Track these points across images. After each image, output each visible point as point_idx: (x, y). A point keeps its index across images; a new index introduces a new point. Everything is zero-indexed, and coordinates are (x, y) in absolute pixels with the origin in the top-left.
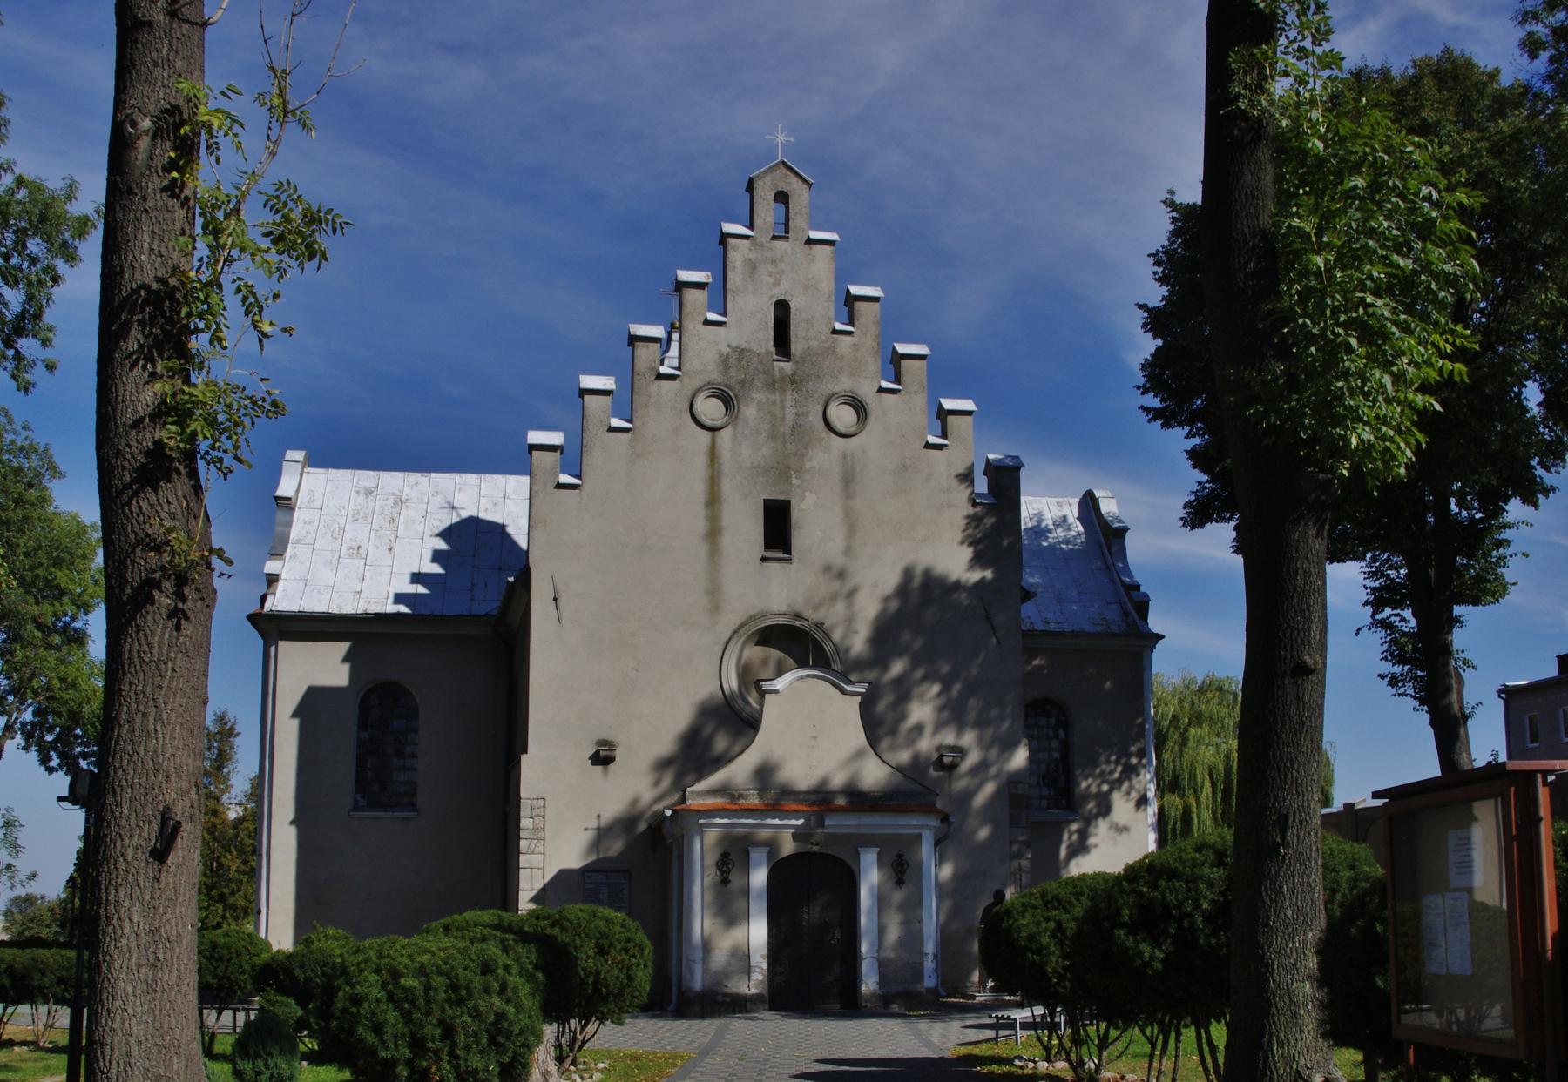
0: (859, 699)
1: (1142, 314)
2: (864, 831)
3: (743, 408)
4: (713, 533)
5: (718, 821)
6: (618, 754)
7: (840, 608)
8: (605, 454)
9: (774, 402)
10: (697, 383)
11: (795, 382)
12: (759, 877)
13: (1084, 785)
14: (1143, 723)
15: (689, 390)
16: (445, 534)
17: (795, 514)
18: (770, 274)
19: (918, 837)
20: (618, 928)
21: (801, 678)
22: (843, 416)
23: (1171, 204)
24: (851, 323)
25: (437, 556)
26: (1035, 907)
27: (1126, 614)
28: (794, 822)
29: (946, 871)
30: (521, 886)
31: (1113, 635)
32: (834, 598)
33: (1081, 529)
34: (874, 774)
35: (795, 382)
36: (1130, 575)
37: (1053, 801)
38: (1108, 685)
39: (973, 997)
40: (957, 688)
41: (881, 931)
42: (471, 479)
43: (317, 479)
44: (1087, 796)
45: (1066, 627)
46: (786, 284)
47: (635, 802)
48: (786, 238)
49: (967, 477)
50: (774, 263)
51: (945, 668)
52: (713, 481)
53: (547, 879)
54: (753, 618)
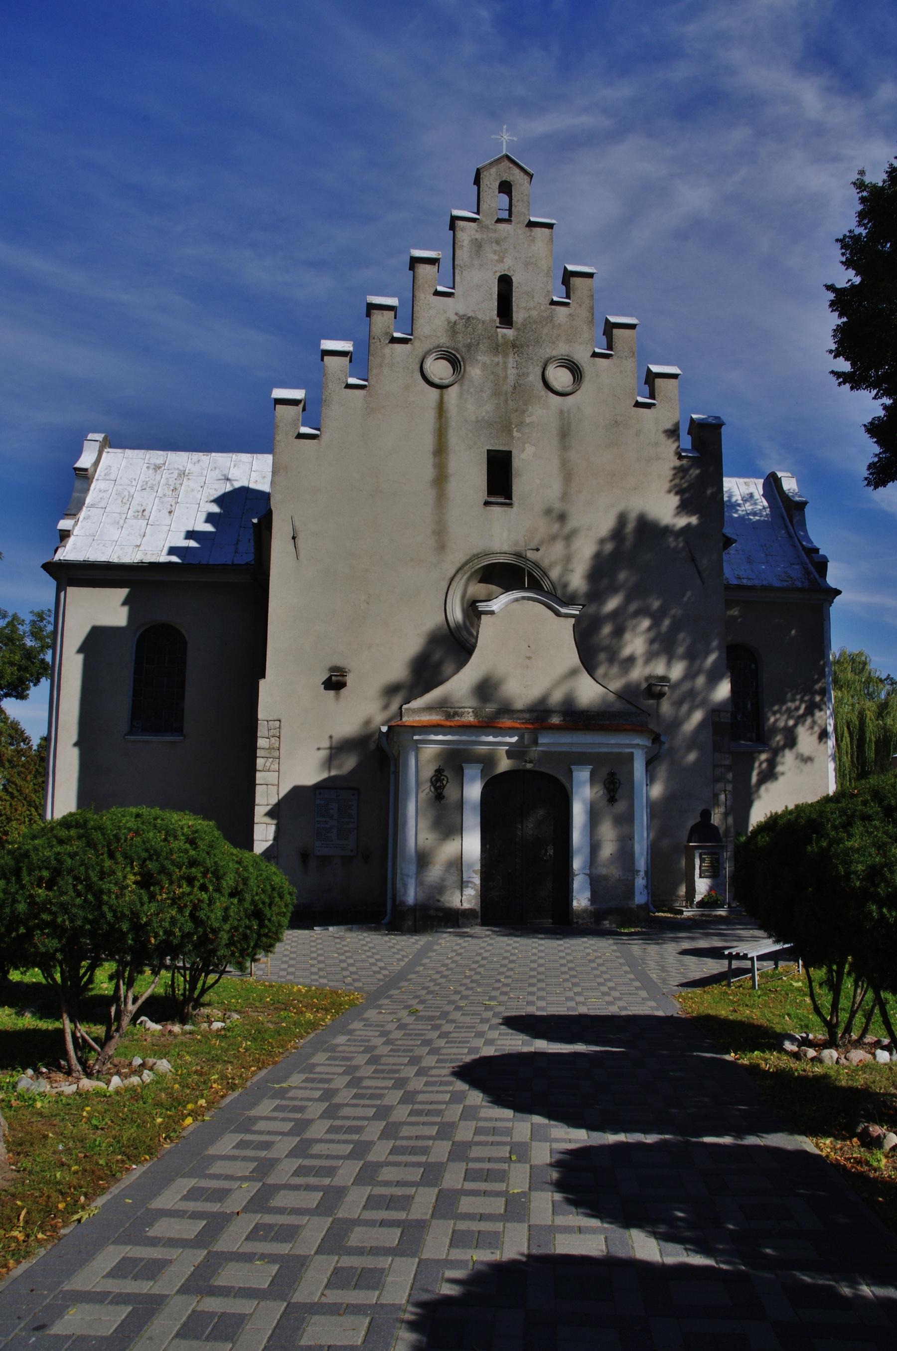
0: (573, 621)
1: (831, 296)
2: (575, 749)
3: (468, 368)
4: (441, 479)
5: (433, 737)
6: (349, 680)
7: (558, 548)
8: (342, 407)
9: (498, 364)
10: (428, 345)
11: (516, 346)
12: (473, 791)
13: (772, 719)
14: (824, 667)
15: (420, 353)
16: (218, 501)
17: (516, 463)
18: (495, 252)
19: (631, 756)
20: (181, 844)
21: (517, 600)
22: (560, 377)
23: (860, 185)
24: (568, 297)
25: (210, 518)
26: (866, 818)
27: (808, 573)
28: (508, 739)
29: (657, 791)
30: (257, 801)
31: (797, 589)
32: (554, 538)
33: (766, 504)
34: (588, 691)
35: (516, 346)
36: (810, 541)
37: (745, 738)
38: (793, 632)
39: (681, 912)
40: (667, 622)
41: (594, 848)
42: (245, 457)
43: (111, 457)
44: (774, 730)
45: (756, 582)
46: (508, 262)
47: (368, 722)
48: (508, 221)
49: (673, 433)
50: (498, 242)
51: (656, 604)
52: (441, 434)
53: (282, 795)
54: (477, 556)
